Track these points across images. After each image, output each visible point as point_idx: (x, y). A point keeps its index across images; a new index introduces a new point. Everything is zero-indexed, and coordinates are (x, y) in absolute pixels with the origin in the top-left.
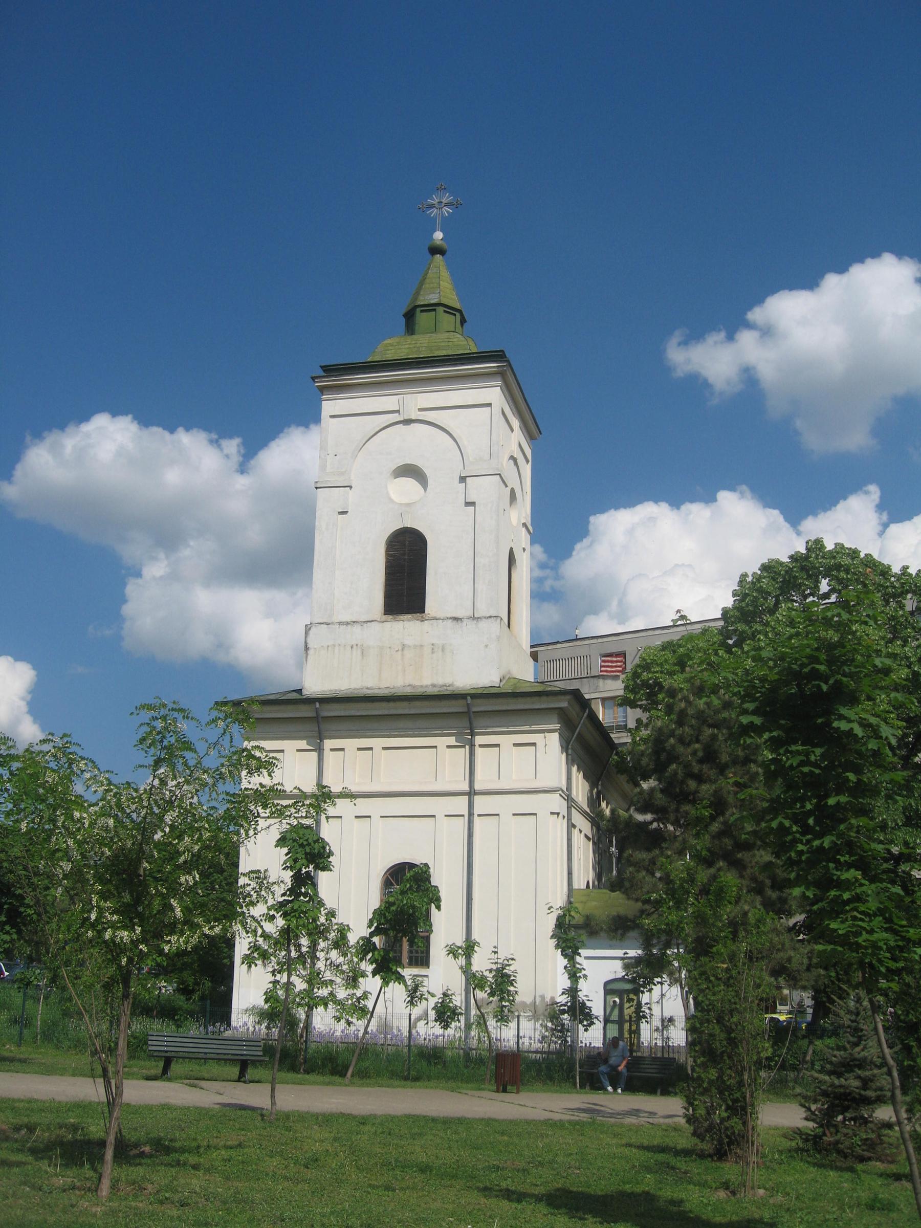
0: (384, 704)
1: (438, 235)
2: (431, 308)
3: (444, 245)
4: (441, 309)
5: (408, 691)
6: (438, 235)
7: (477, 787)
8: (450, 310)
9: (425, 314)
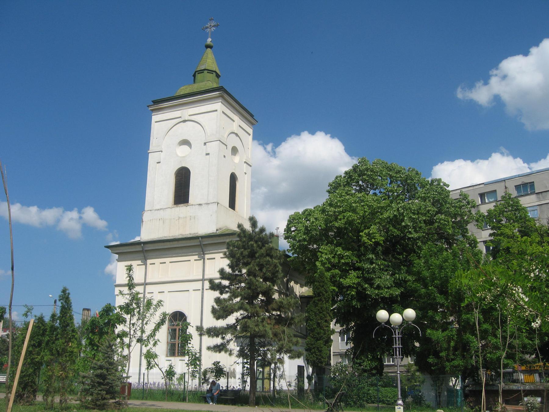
0: (168, 243)
1: (209, 40)
2: (202, 71)
3: (212, 44)
4: (206, 71)
5: (180, 237)
6: (209, 40)
7: (201, 278)
8: (211, 71)
9: (199, 75)
